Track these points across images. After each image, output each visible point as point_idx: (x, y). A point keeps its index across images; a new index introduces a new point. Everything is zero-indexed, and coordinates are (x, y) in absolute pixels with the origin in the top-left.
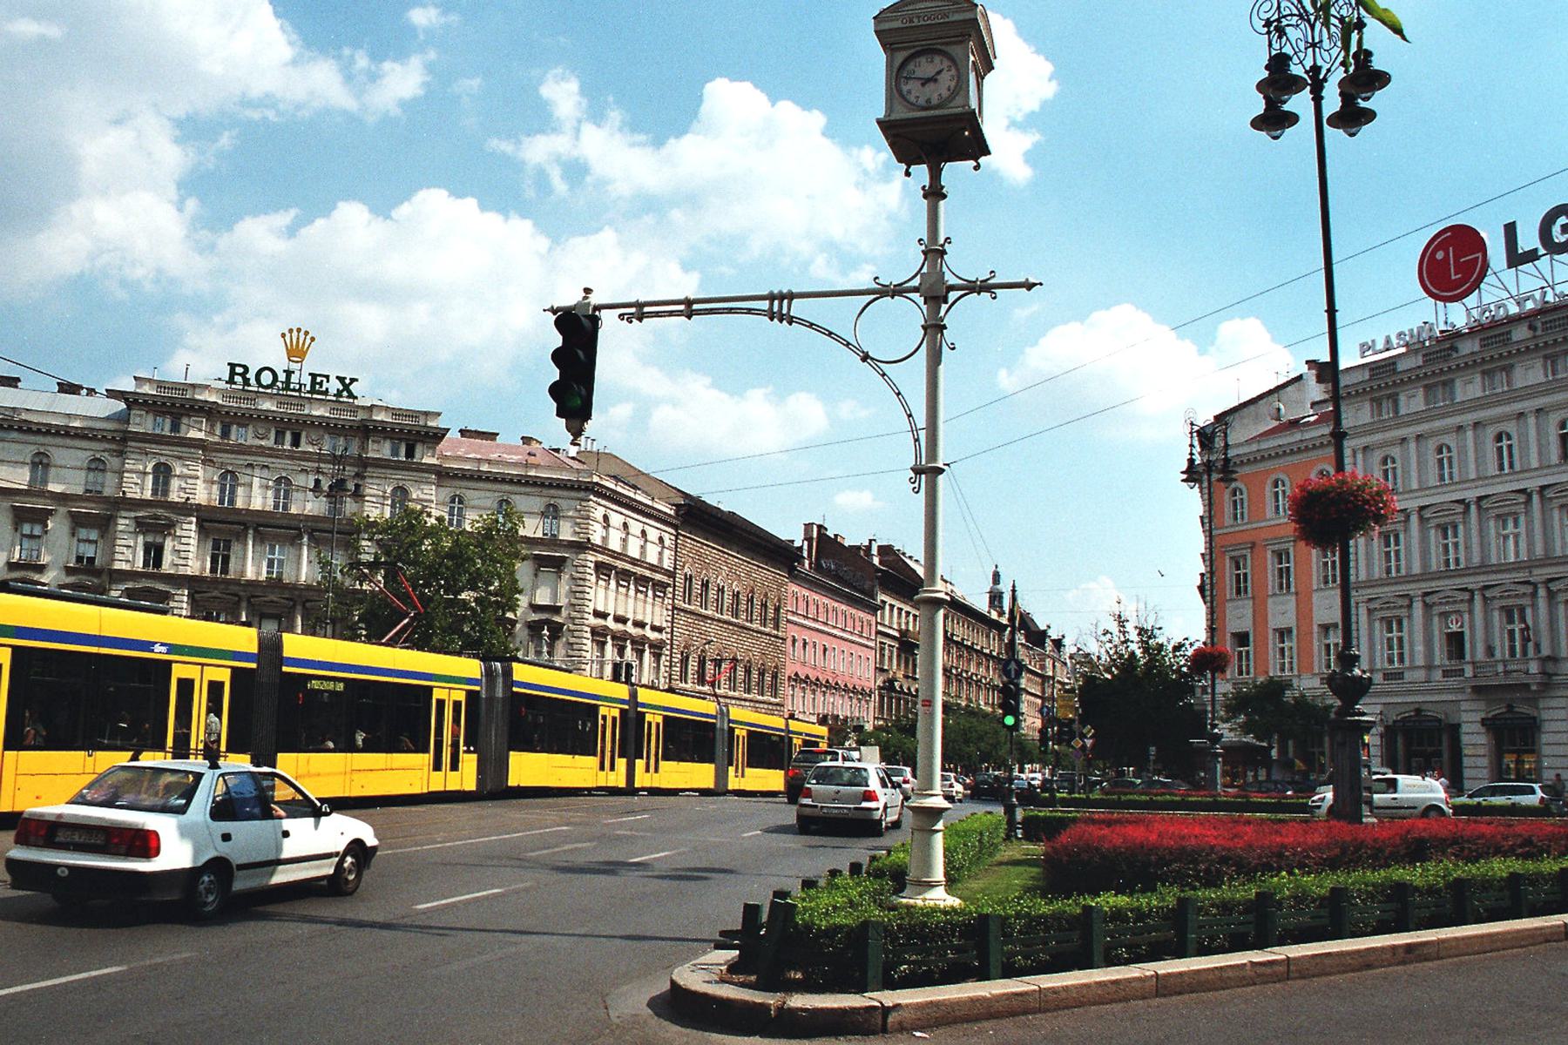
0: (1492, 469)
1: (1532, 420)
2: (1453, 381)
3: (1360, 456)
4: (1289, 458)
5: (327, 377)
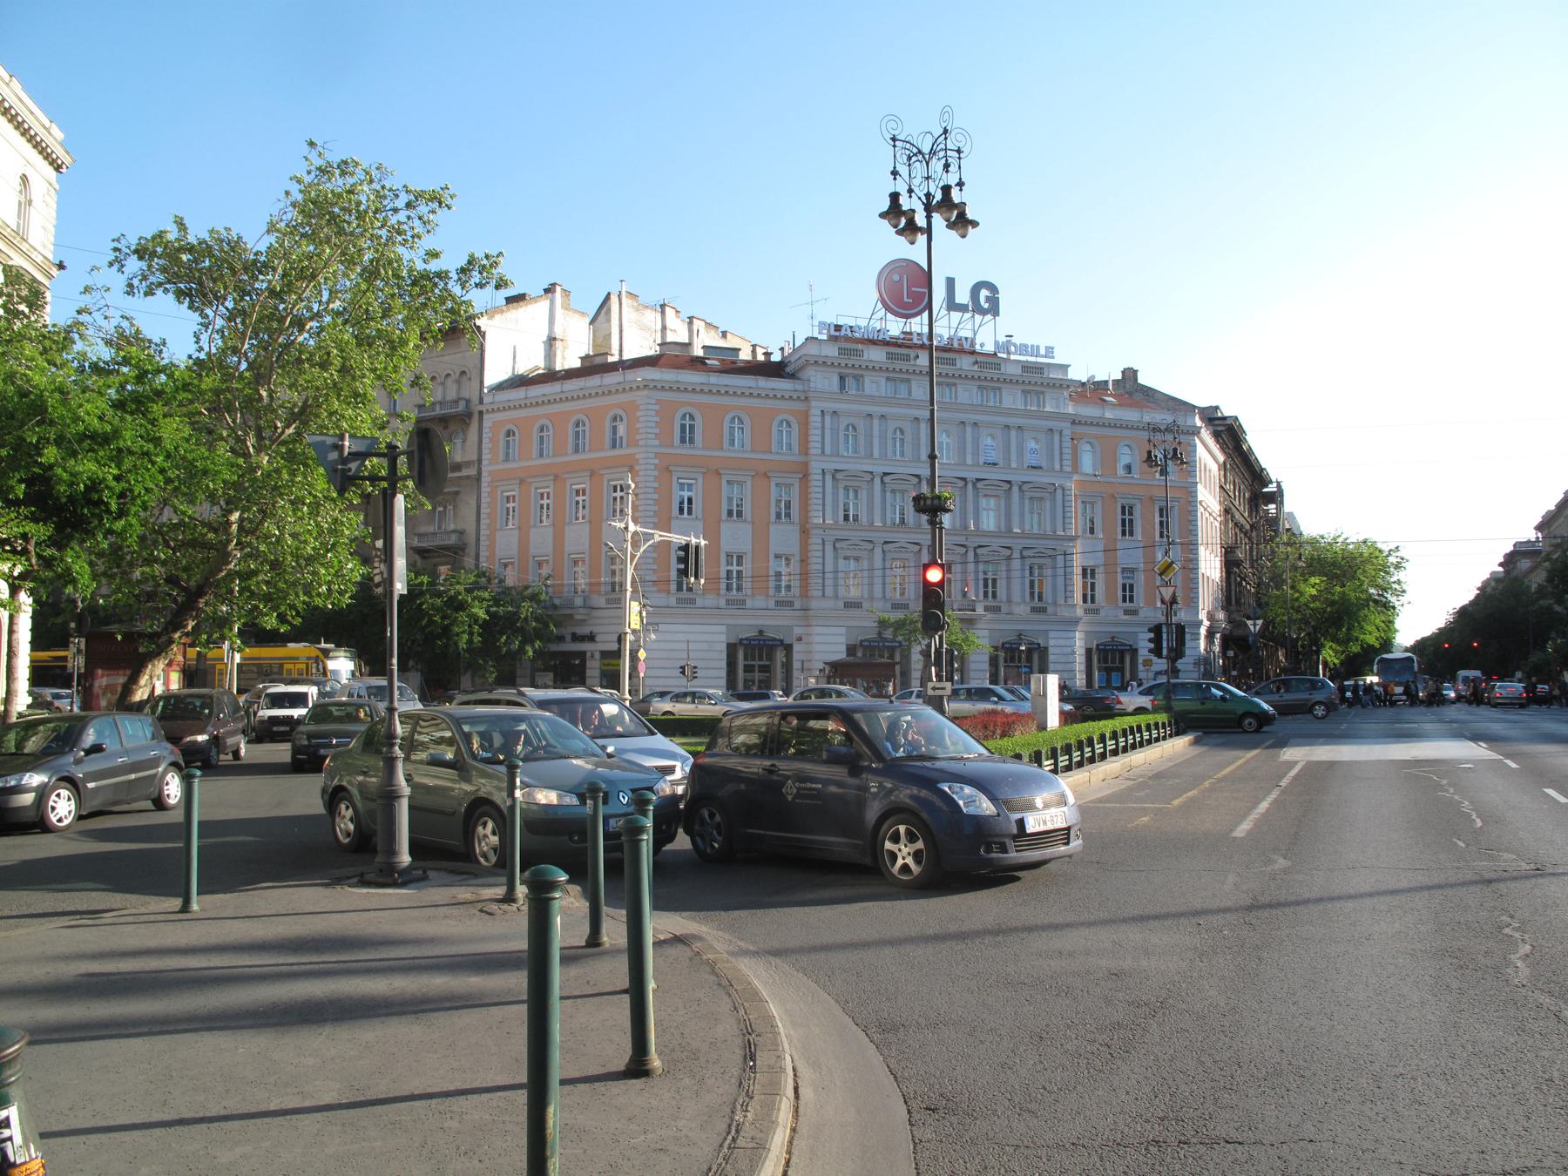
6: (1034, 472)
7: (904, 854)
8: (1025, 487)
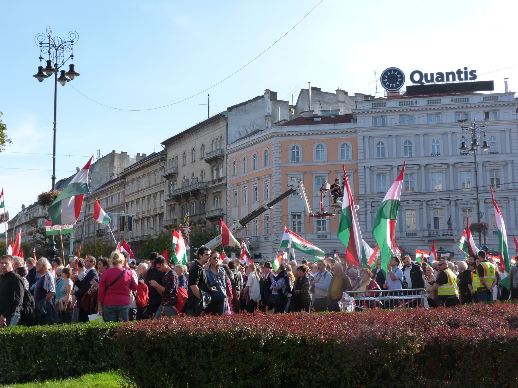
1: (394, 139)
3: (367, 140)
4: (332, 136)
6: (493, 155)
8: (373, 169)
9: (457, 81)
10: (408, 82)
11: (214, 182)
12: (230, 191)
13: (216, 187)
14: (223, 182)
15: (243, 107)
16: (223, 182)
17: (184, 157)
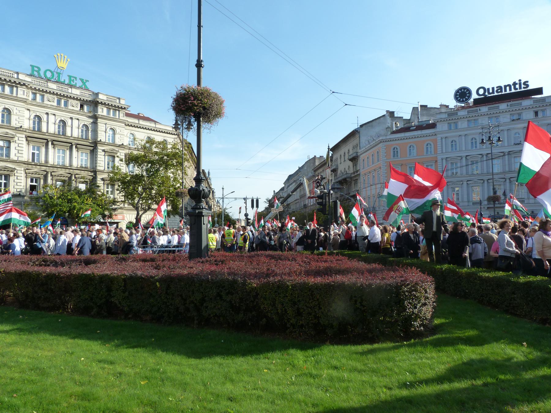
0: (450, 150)
1: (463, 137)
2: (478, 119)
5: (76, 78)
7: (425, 303)
9: (513, 91)
10: (474, 96)
11: (354, 173)
12: (361, 179)
13: (355, 176)
14: (359, 173)
15: (371, 124)
16: (359, 173)
17: (340, 158)
